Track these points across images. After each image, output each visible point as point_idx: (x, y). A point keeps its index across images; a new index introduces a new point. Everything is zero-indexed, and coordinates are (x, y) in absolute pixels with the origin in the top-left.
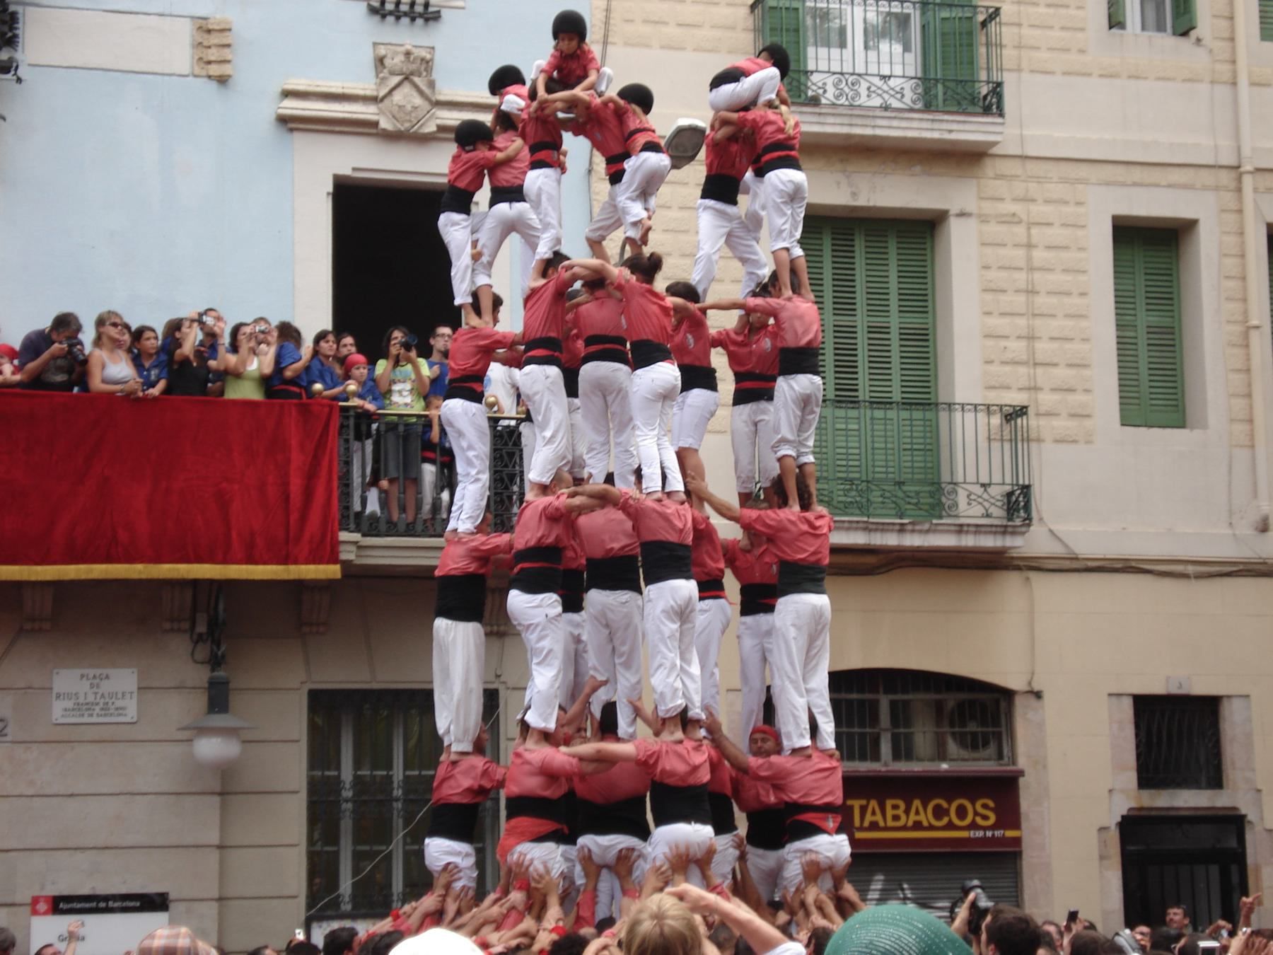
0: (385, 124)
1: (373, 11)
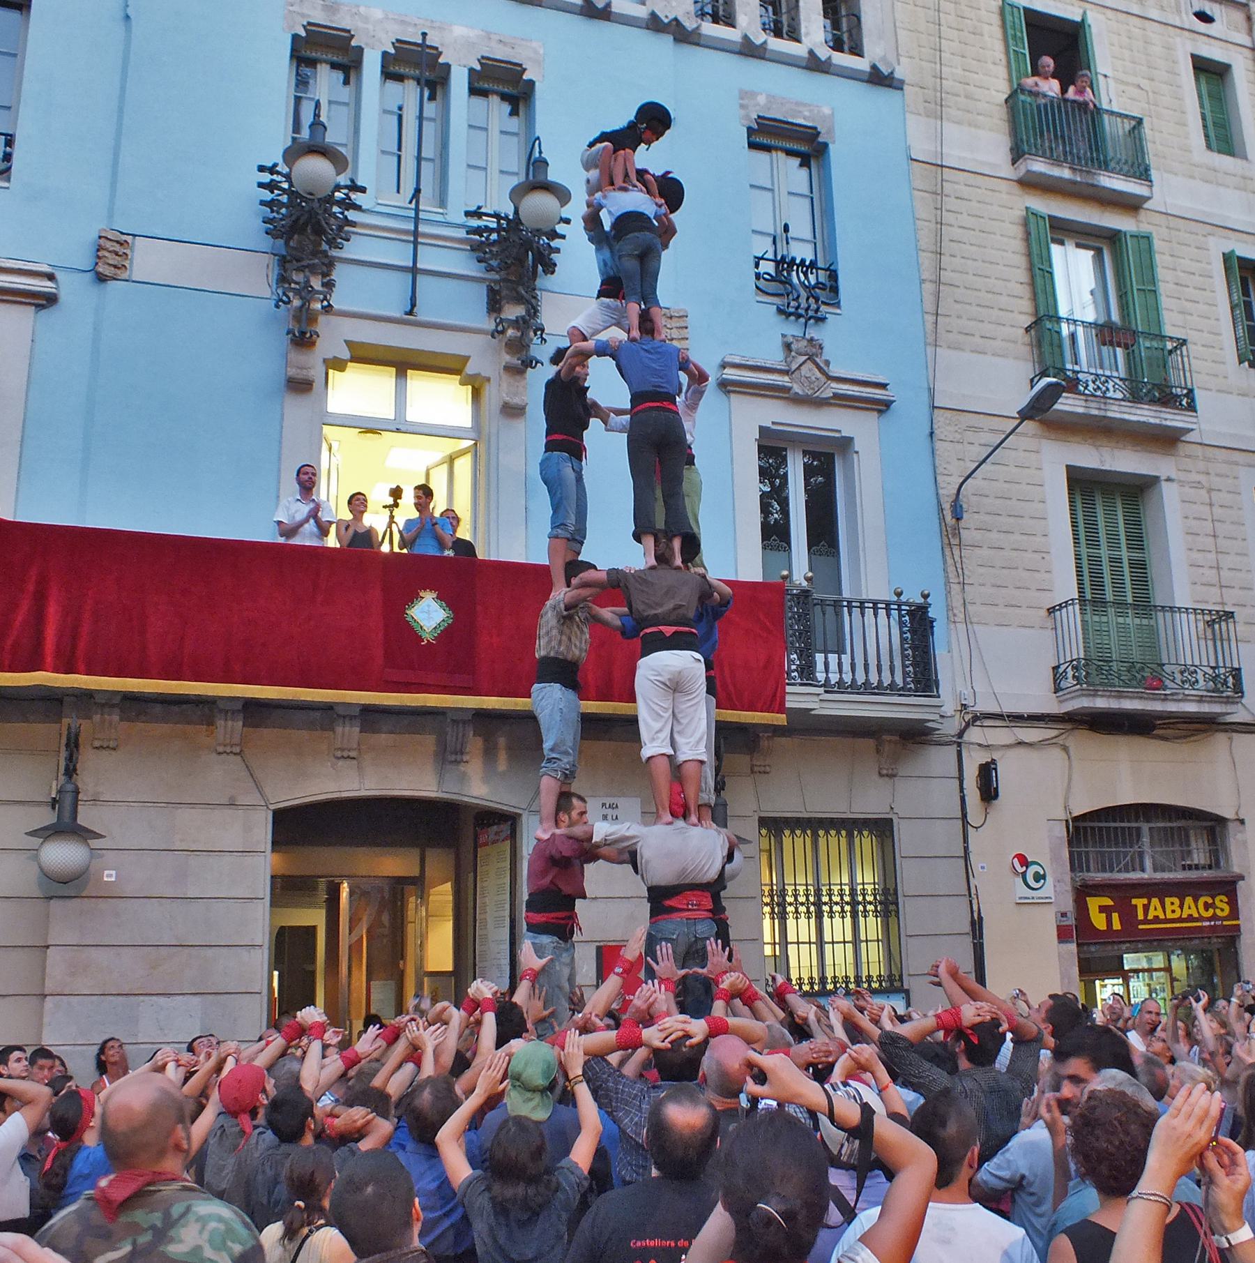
0: (797, 389)
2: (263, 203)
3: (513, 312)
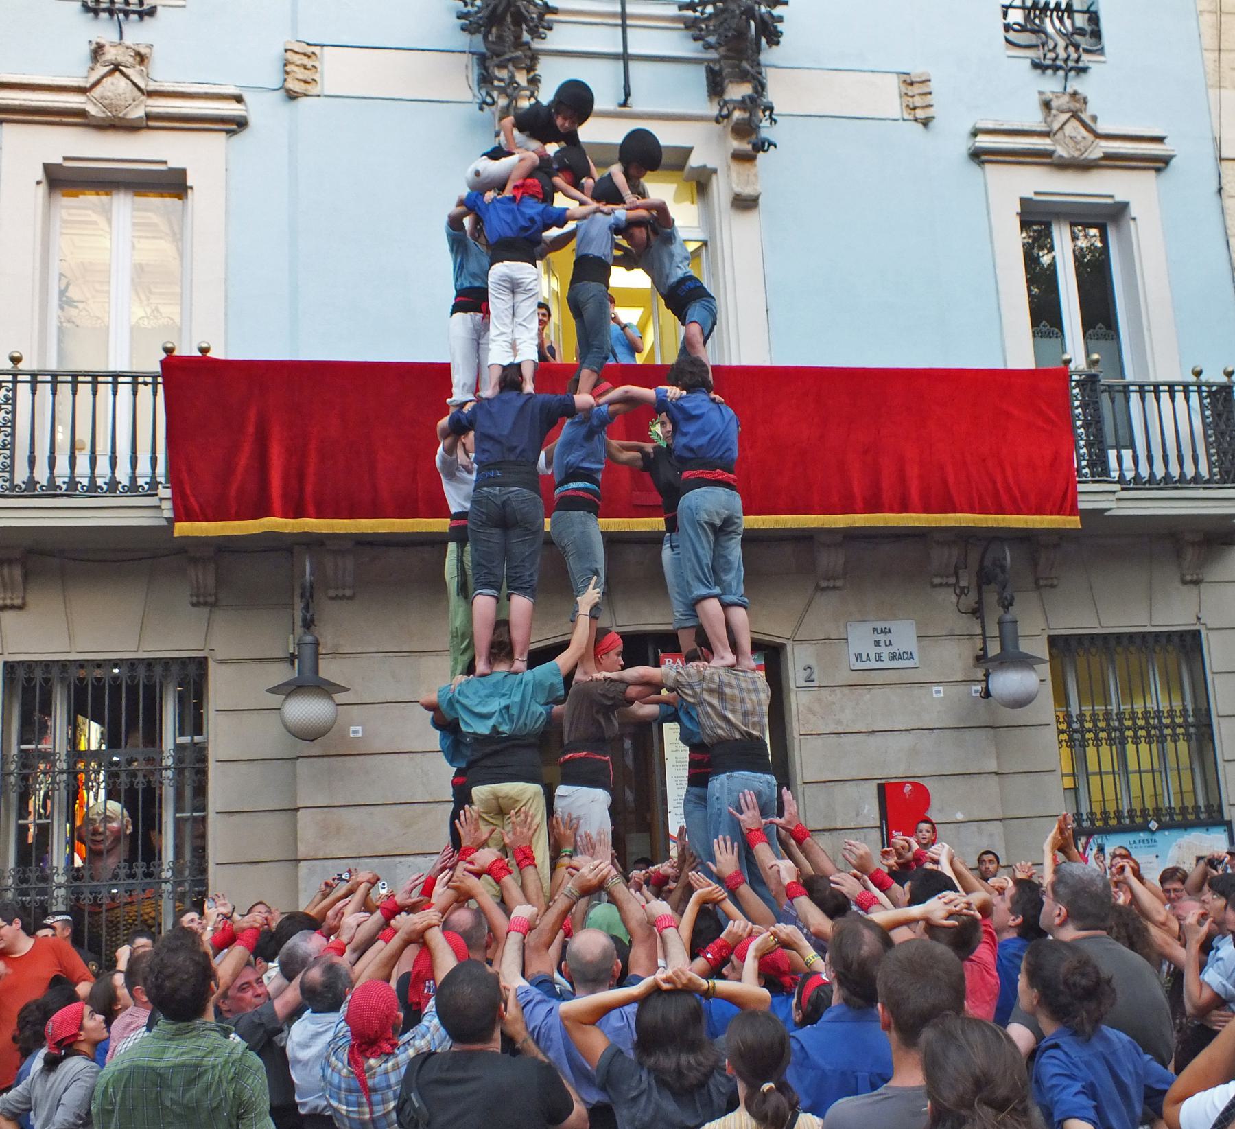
1: (87, 9)
3: (738, 91)
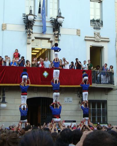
0: (96, 40)
1: (94, 28)
2: (23, 18)
